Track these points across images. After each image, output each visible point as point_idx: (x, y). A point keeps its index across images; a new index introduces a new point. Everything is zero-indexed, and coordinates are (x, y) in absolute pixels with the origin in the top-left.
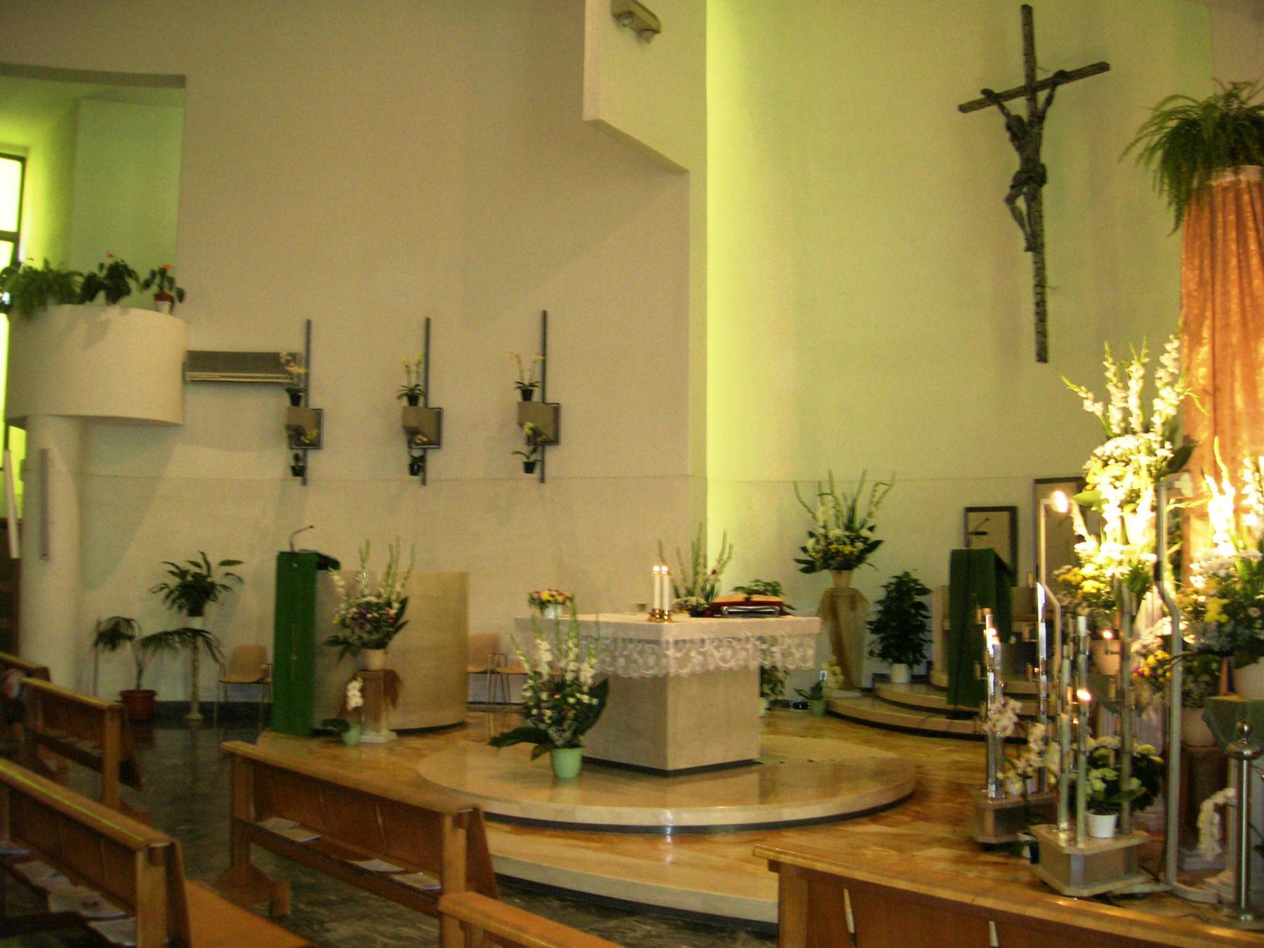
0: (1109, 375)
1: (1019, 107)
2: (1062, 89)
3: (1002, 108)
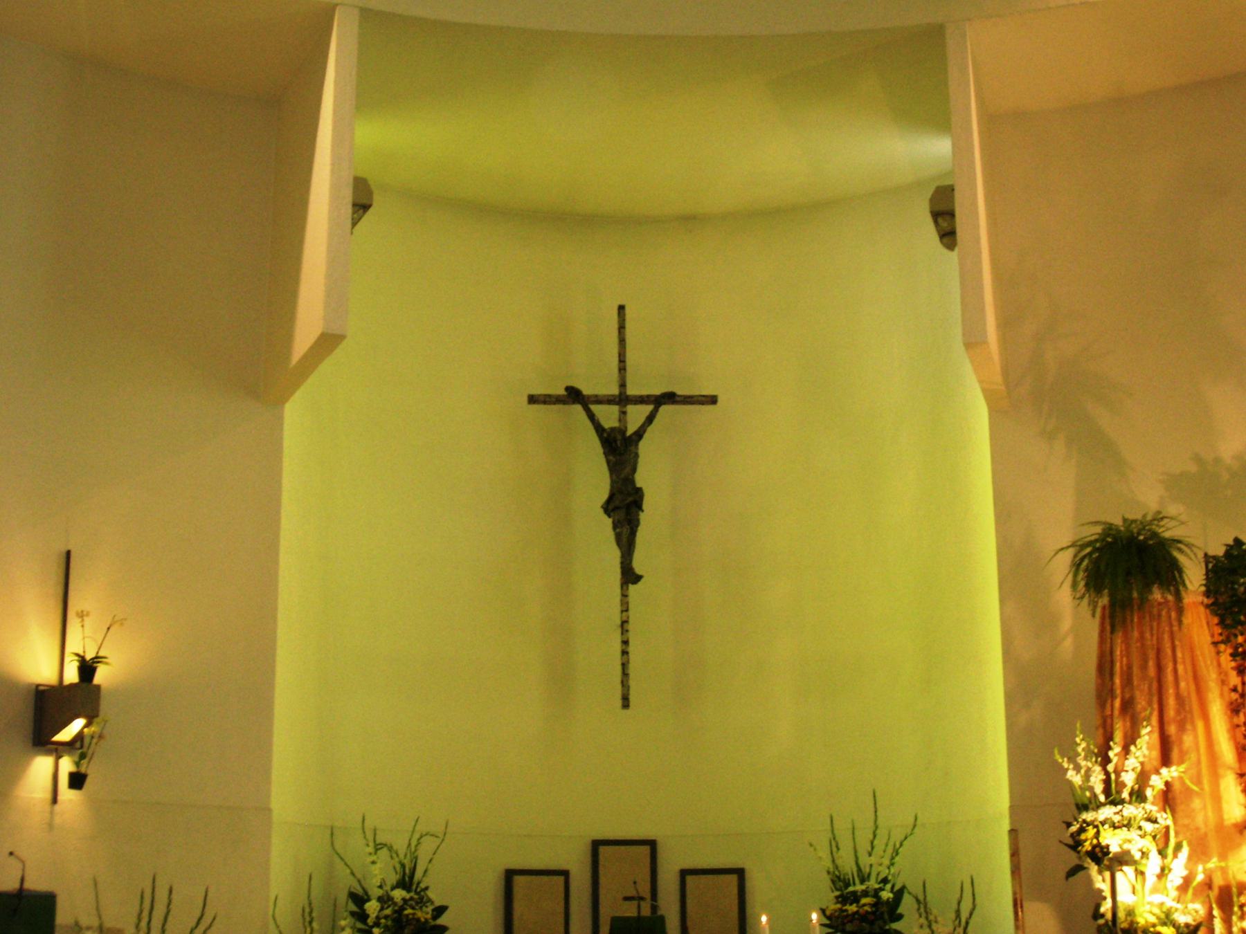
0: (1080, 749)
1: (608, 416)
2: (664, 409)
3: (591, 417)
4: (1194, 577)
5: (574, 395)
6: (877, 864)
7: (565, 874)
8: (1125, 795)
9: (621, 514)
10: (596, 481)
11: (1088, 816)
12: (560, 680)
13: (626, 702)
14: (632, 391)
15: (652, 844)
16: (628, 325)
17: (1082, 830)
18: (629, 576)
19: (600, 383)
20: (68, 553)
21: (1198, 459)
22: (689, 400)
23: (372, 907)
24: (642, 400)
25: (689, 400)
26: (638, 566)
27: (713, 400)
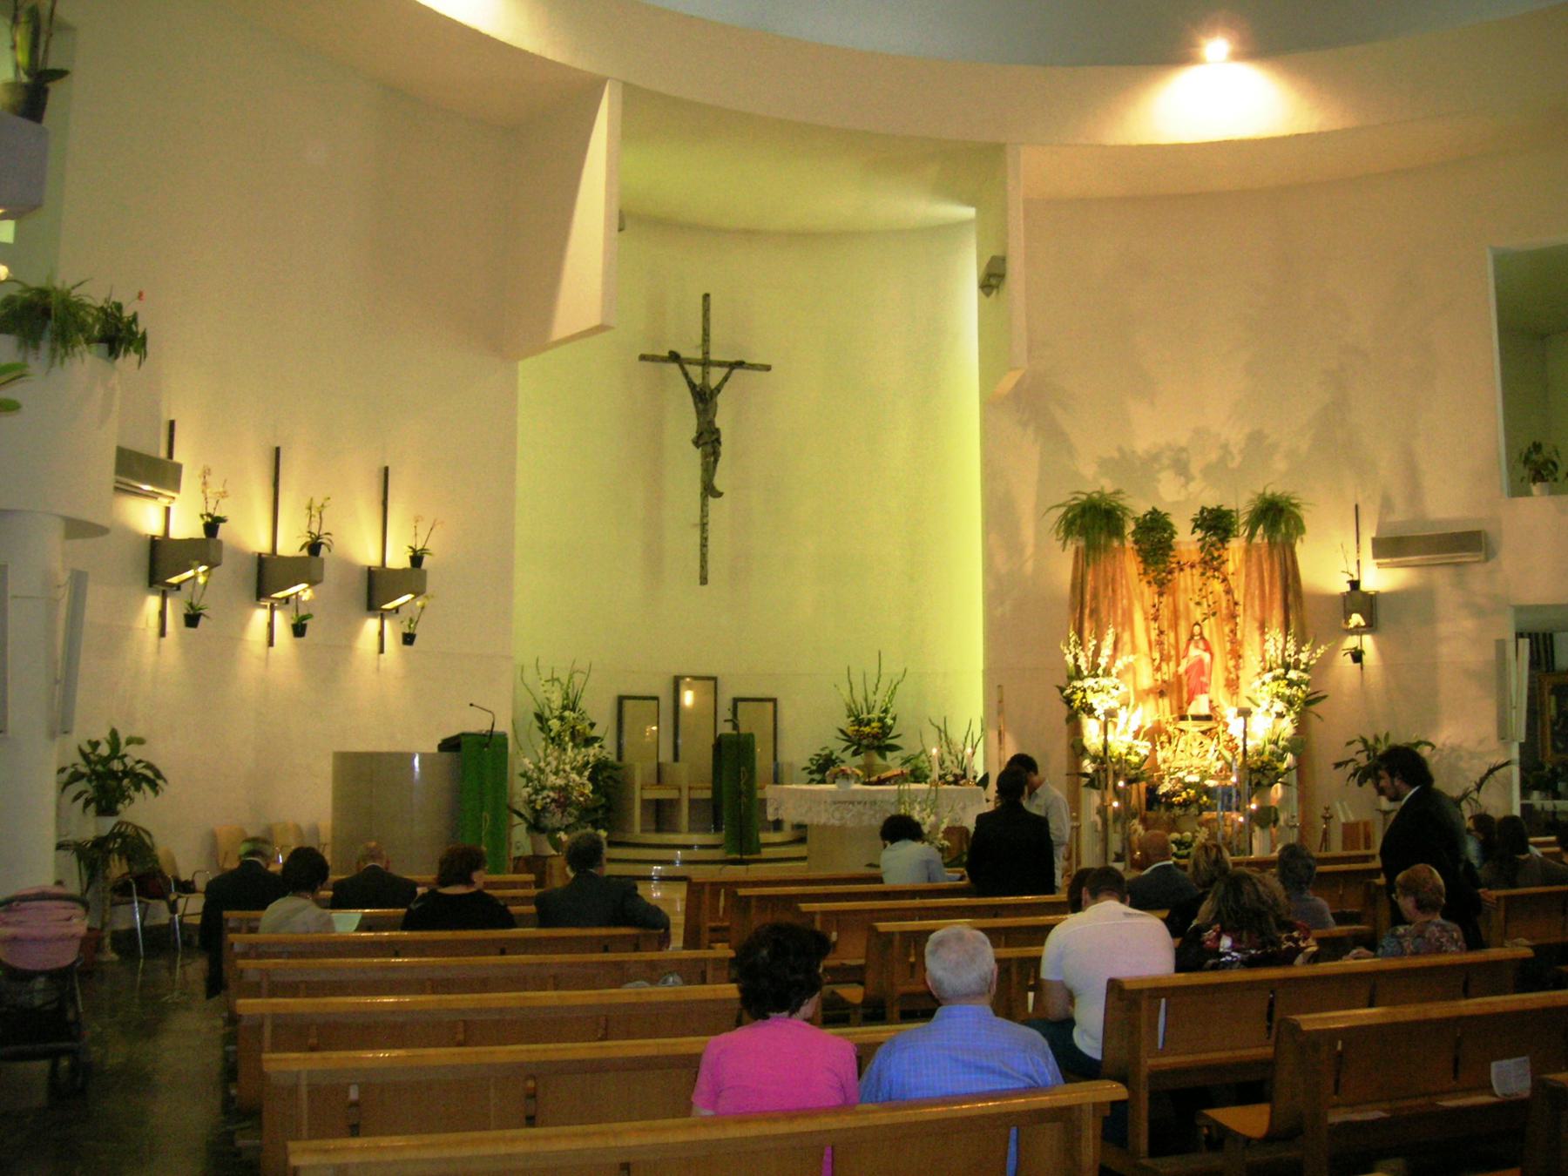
2: (736, 372)
3: (686, 375)
4: (1130, 527)
5: (674, 357)
6: (879, 700)
7: (656, 698)
8: (1100, 672)
9: (709, 449)
10: (686, 421)
11: (1078, 684)
12: (654, 560)
13: (704, 580)
14: (714, 357)
15: (715, 679)
16: (712, 311)
17: (1073, 693)
18: (709, 490)
19: (690, 351)
20: (386, 469)
21: (1120, 449)
22: (753, 367)
23: (555, 724)
24: (721, 364)
25: (753, 367)
26: (719, 483)
27: (768, 368)
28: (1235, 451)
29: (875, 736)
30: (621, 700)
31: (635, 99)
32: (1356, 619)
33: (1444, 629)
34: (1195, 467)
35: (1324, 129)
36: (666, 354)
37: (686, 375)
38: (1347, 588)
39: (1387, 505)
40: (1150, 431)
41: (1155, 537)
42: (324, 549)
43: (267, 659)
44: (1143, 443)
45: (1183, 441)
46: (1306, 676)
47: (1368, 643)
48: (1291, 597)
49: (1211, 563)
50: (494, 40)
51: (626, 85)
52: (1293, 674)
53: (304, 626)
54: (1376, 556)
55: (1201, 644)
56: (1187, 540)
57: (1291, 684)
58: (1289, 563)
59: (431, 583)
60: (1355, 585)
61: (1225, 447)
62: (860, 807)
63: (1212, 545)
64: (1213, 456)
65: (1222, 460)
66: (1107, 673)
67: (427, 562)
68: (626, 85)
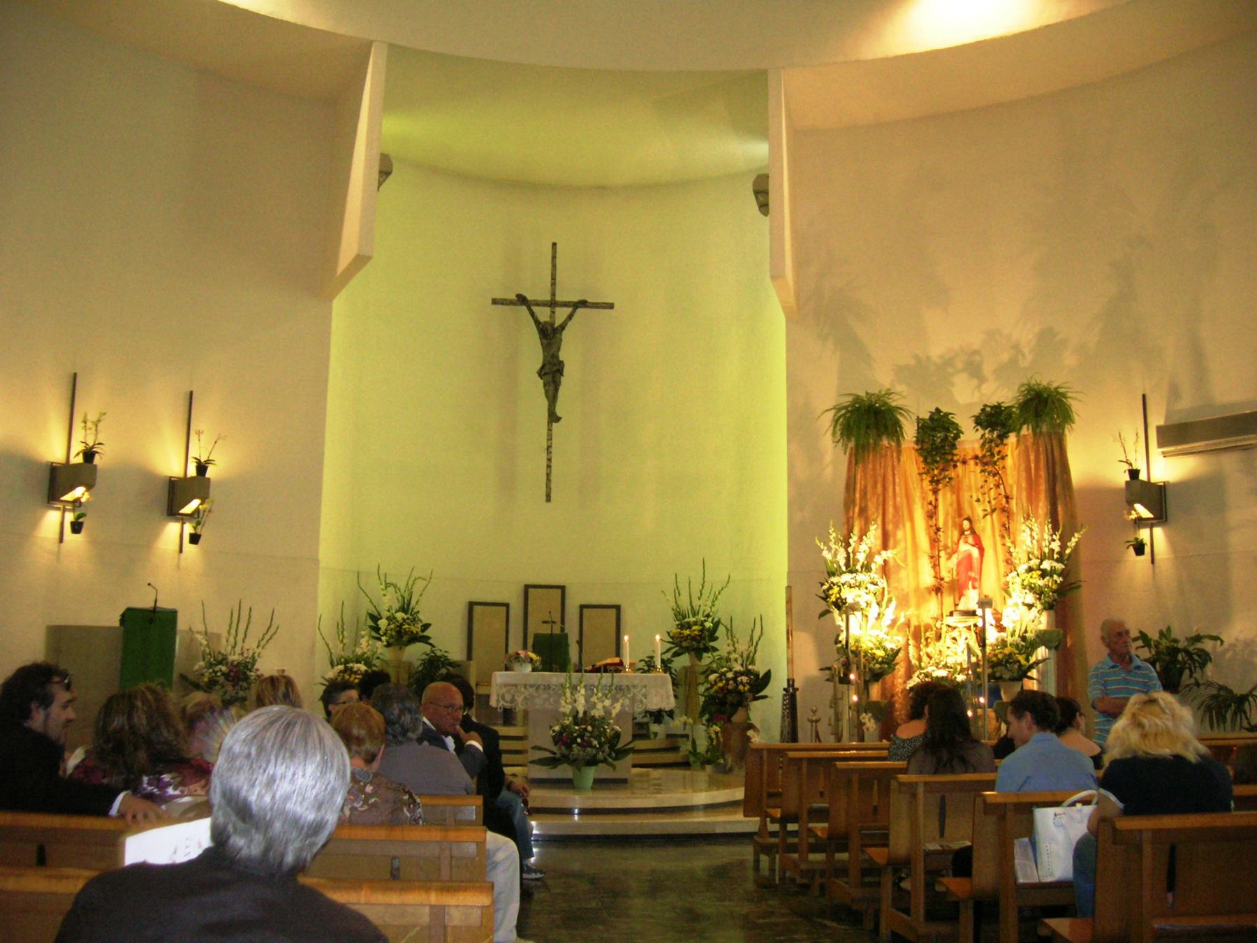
2: (580, 311)
3: (532, 314)
5: (522, 300)
6: (704, 605)
7: (507, 605)
10: (533, 355)
11: (834, 579)
12: (507, 483)
15: (563, 588)
17: (830, 588)
18: (553, 418)
20: (75, 375)
21: (916, 357)
24: (565, 304)
26: (559, 411)
27: (611, 306)
28: (1026, 351)
29: (694, 638)
30: (471, 605)
31: (397, 53)
32: (1142, 511)
33: (1235, 516)
34: (987, 370)
35: (1072, 16)
36: (513, 297)
37: (532, 314)
38: (1127, 478)
39: (1174, 392)
40: (944, 336)
41: (938, 438)
42: (97, 458)
43: (59, 552)
44: (937, 350)
45: (976, 345)
46: (1059, 566)
47: (1158, 538)
48: (1058, 488)
49: (989, 460)
50: (257, 14)
51: (392, 47)
52: (1046, 565)
53: (81, 524)
54: (1160, 445)
55: (971, 540)
56: (971, 439)
57: (1044, 574)
58: (1056, 454)
59: (213, 492)
60: (1134, 474)
61: (1016, 348)
62: (532, 690)
63: (991, 441)
64: (1005, 357)
65: (1013, 362)
66: (867, 568)
67: (211, 473)
68: (392, 47)
